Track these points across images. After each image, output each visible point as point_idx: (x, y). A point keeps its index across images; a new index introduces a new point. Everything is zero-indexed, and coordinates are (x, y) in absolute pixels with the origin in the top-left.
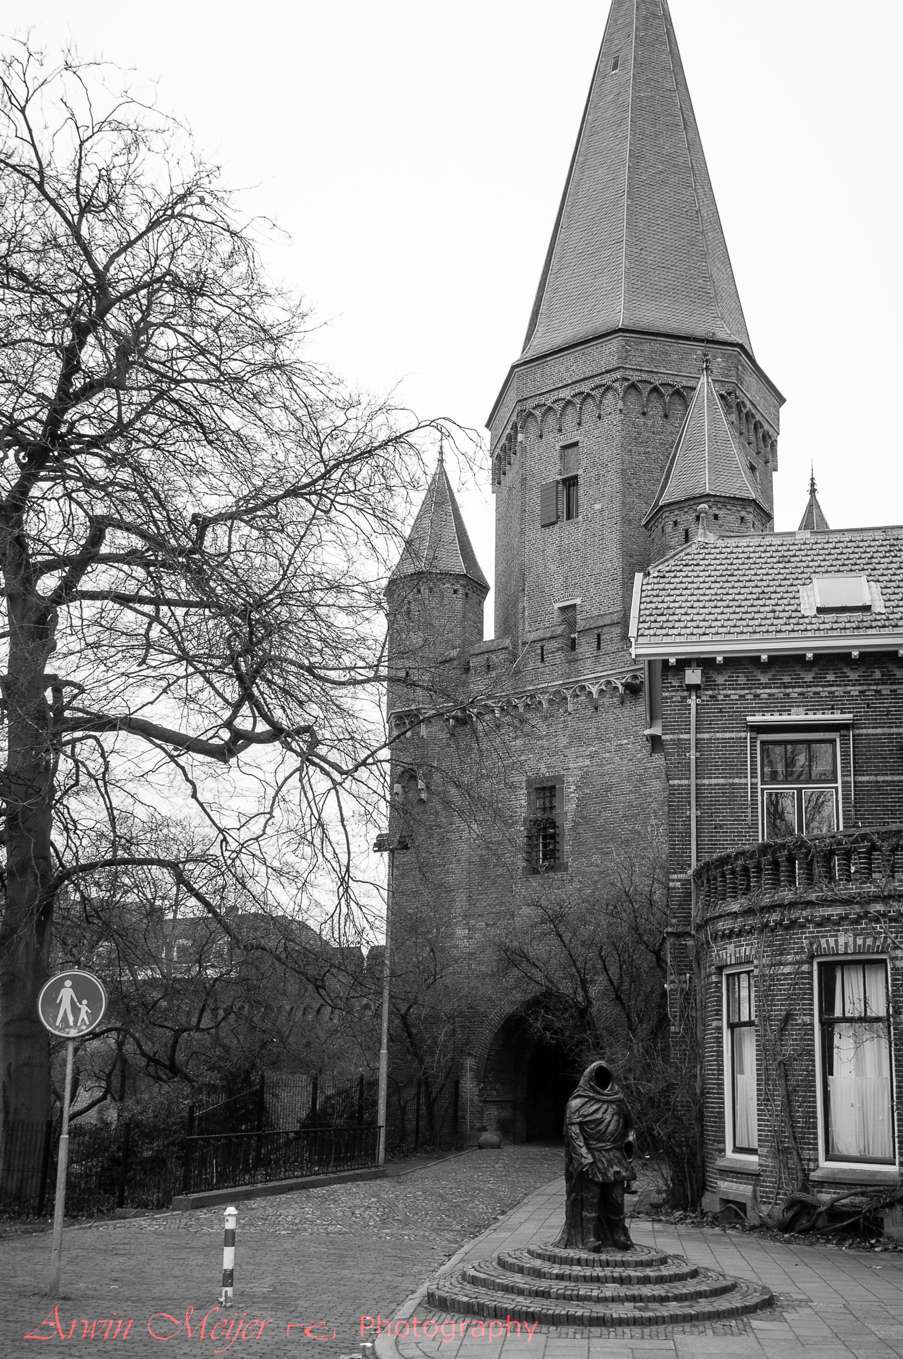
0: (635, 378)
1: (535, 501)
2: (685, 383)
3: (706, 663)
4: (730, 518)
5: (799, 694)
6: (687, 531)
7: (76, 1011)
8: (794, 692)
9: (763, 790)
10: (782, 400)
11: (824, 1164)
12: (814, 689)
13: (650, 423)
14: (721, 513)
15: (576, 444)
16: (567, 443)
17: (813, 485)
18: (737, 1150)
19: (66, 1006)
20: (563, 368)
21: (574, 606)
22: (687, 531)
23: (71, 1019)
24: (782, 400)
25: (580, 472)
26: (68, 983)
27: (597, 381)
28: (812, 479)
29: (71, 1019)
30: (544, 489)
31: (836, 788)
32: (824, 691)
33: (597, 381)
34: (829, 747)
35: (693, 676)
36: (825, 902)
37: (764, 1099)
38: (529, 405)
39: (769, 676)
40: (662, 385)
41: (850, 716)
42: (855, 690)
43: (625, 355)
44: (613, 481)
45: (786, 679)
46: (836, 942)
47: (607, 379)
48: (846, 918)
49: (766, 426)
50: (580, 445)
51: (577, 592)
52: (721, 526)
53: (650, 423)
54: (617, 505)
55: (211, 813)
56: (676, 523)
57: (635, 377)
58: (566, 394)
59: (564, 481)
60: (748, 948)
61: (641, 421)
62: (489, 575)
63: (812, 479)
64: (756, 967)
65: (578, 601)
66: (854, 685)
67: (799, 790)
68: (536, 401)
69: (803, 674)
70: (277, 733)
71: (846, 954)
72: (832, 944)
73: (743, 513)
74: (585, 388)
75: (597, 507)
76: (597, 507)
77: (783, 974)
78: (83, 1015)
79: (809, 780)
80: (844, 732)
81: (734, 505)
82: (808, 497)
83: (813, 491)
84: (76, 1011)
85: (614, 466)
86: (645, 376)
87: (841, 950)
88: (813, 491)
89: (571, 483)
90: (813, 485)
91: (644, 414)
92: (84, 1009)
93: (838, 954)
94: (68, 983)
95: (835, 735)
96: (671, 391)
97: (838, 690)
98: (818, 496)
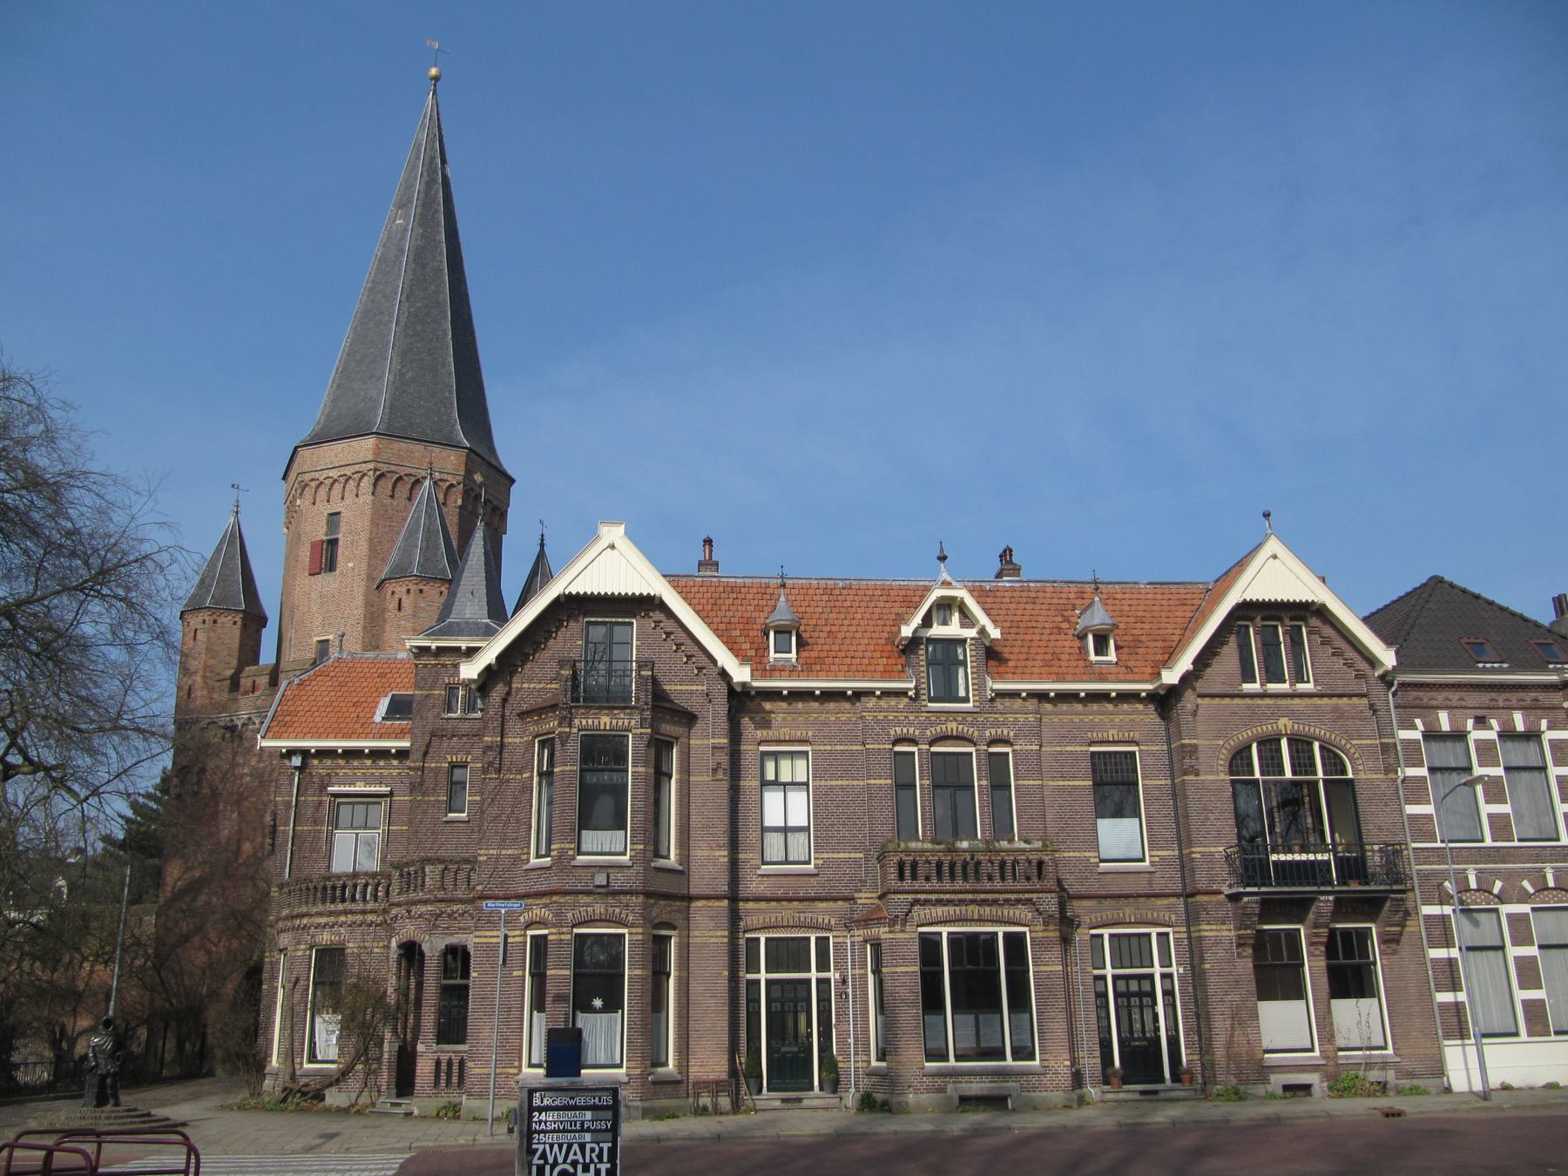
1: (305, 553)
3: (305, 753)
8: (359, 773)
10: (513, 481)
11: (306, 1066)
18: (531, 1065)
24: (513, 481)
27: (357, 468)
30: (313, 545)
32: (377, 772)
33: (357, 468)
35: (297, 761)
36: (320, 914)
38: (307, 477)
42: (395, 772)
43: (378, 451)
44: (363, 547)
47: (364, 467)
54: (364, 566)
57: (385, 468)
58: (334, 474)
59: (329, 541)
61: (389, 500)
68: (312, 475)
70: (36, 766)
74: (348, 471)
79: (366, 828)
83: (542, 545)
85: (365, 535)
86: (393, 468)
88: (542, 545)
89: (333, 543)
91: (392, 497)
97: (385, 772)
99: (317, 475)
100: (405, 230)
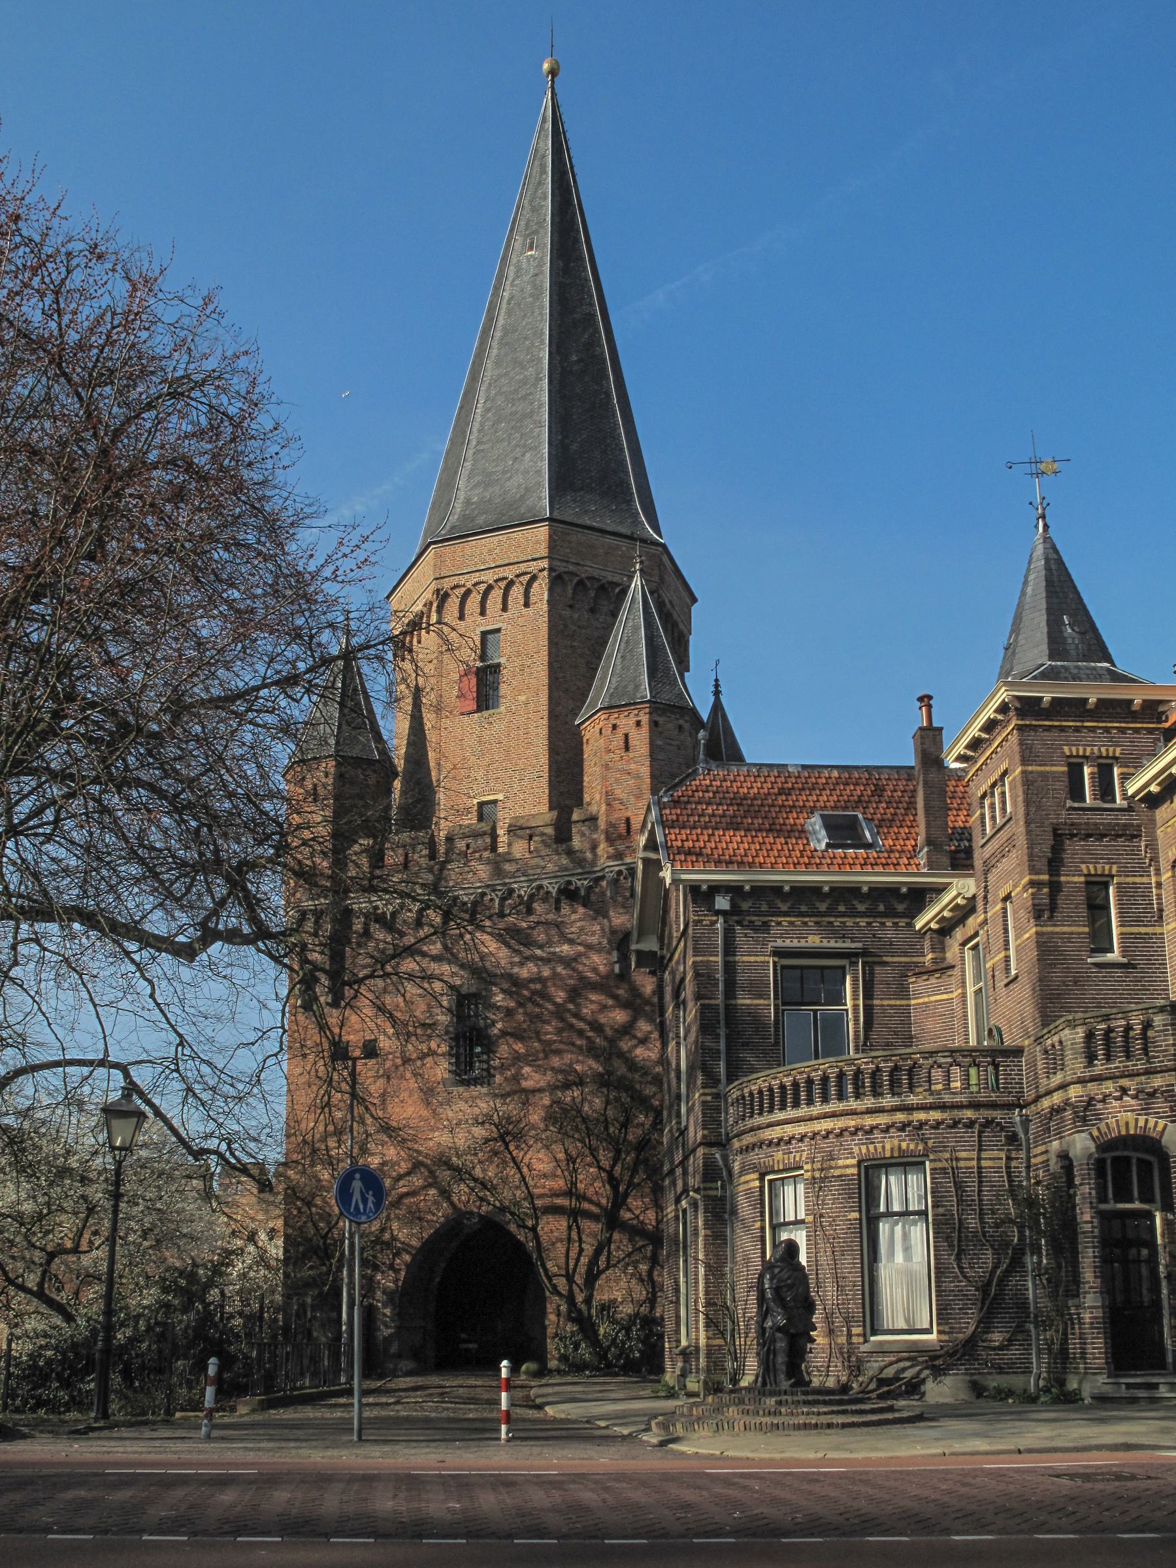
0: (562, 569)
2: (610, 578)
4: (670, 726)
5: (816, 923)
6: (626, 736)
7: (365, 1201)
9: (783, 1011)
10: (694, 600)
12: (828, 919)
13: (576, 616)
14: (661, 720)
15: (498, 630)
16: (488, 628)
17: (717, 686)
19: (357, 1196)
20: (485, 551)
21: (495, 802)
22: (626, 736)
23: (361, 1207)
24: (694, 600)
25: (503, 660)
26: (357, 1176)
28: (717, 680)
29: (361, 1207)
31: (847, 1010)
33: (523, 567)
34: (840, 971)
37: (291, 1409)
39: (789, 904)
40: (588, 578)
41: (860, 945)
45: (804, 908)
46: (883, 1147)
47: (533, 567)
48: (893, 1125)
49: (681, 626)
50: (503, 632)
51: (498, 786)
52: (661, 733)
53: (576, 616)
55: (169, 1015)
56: (614, 727)
60: (798, 1155)
62: (400, 763)
63: (717, 680)
64: (807, 1171)
65: (500, 797)
66: (862, 917)
67: (815, 1011)
68: (455, 581)
69: (818, 904)
71: (892, 1157)
72: (880, 1150)
73: (681, 722)
75: (522, 698)
76: (522, 698)
77: (833, 1177)
78: (370, 1205)
80: (854, 959)
81: (672, 713)
82: (712, 699)
83: (717, 693)
84: (365, 1201)
86: (571, 568)
87: (888, 1154)
88: (717, 693)
90: (717, 686)
92: (371, 1199)
93: (860, 1219)
94: (357, 1176)
95: (845, 962)
96: (596, 585)
98: (723, 698)
99: (462, 580)
100: (540, 265)
